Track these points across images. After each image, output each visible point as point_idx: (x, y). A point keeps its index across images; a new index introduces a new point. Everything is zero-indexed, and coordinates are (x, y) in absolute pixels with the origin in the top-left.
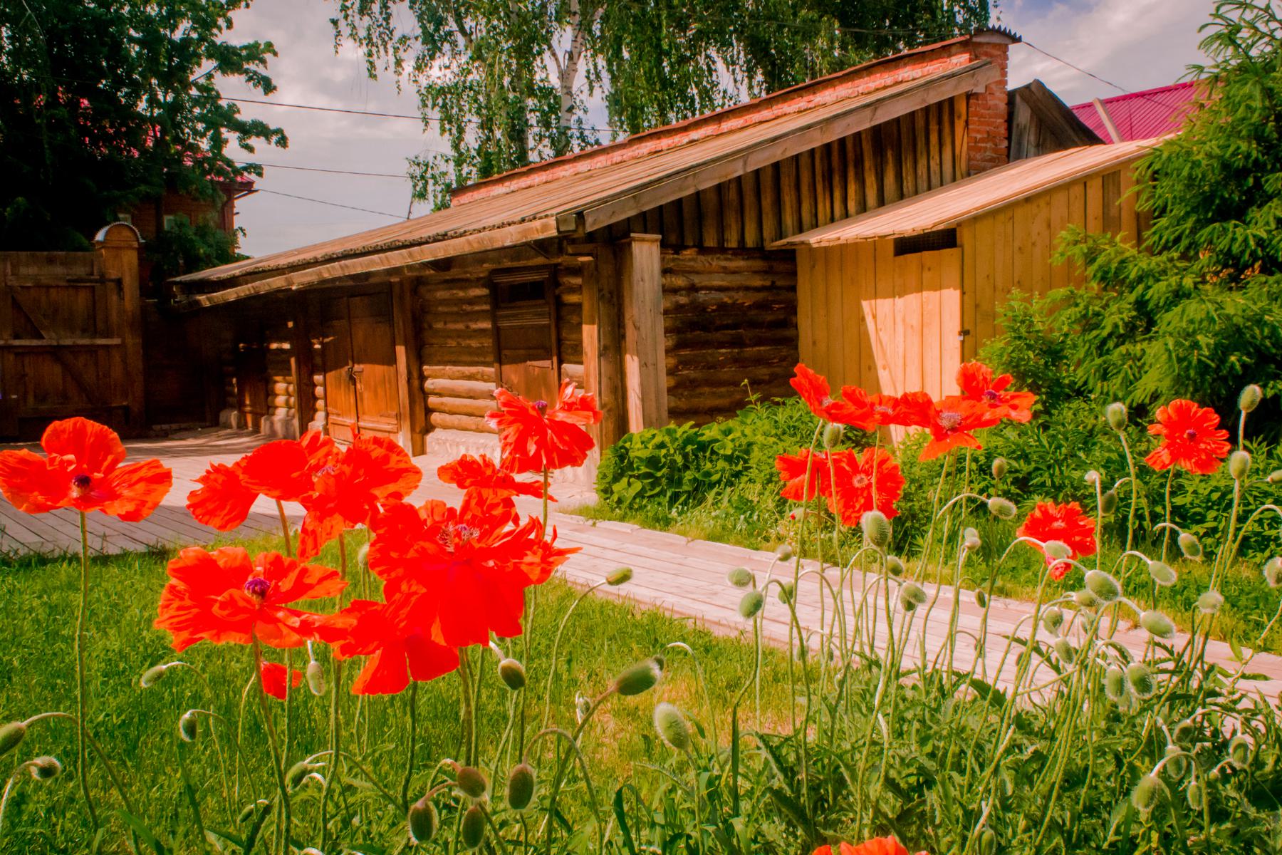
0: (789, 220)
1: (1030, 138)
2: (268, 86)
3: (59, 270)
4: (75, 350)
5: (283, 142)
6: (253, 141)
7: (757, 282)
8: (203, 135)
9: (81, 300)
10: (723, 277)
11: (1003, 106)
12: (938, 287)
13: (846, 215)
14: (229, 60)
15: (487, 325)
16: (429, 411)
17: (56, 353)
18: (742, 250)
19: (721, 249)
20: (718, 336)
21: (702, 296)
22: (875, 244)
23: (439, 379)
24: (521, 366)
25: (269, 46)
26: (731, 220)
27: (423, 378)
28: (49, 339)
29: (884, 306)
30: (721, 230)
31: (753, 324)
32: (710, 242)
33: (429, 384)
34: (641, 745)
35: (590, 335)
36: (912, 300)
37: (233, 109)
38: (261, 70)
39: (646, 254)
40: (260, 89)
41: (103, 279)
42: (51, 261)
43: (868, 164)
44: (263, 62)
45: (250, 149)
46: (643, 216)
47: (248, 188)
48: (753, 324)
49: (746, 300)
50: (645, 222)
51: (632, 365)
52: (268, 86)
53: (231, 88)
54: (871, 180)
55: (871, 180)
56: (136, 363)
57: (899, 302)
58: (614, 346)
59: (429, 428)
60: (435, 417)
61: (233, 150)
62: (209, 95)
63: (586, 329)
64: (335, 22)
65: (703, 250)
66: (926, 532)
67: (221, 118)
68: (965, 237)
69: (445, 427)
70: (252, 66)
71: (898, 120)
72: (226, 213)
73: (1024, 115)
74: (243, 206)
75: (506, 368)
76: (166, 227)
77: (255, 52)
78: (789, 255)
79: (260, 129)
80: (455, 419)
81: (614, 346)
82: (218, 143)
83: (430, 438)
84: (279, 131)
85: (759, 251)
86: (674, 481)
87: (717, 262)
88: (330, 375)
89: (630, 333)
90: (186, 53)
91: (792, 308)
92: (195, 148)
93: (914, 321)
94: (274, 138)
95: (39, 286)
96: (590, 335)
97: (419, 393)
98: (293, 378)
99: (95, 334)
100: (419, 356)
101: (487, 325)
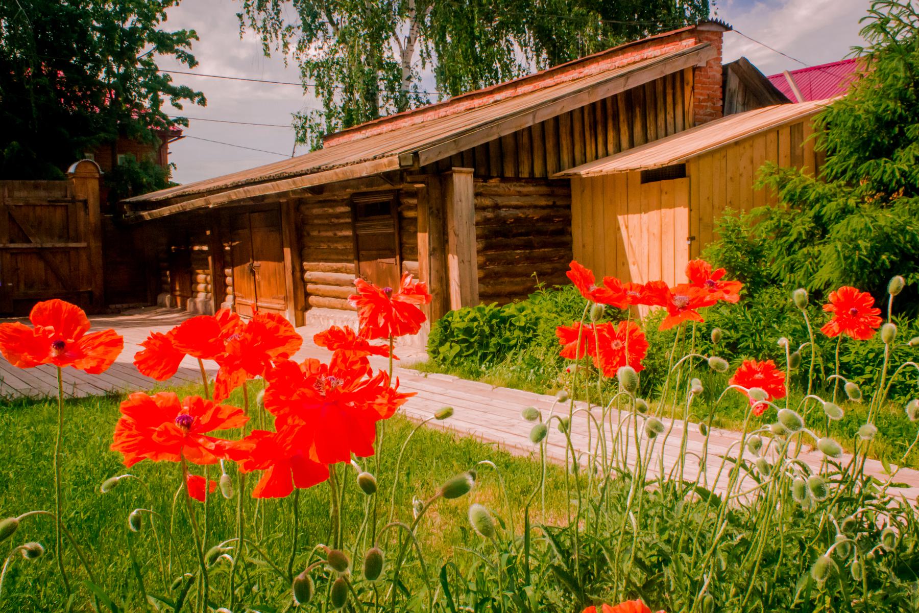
0: (565, 158)
1: (739, 99)
2: (192, 62)
3: (42, 194)
4: (54, 251)
5: (203, 102)
6: (181, 101)
7: (543, 202)
8: (145, 97)
9: (58, 215)
10: (518, 199)
11: (719, 76)
12: (672, 206)
13: (607, 154)
14: (164, 43)
15: (349, 233)
16: (307, 295)
17: (40, 253)
18: (532, 180)
19: (517, 179)
20: (515, 241)
21: (503, 212)
22: (627, 175)
23: (315, 272)
24: (374, 263)
25: (193, 33)
26: (524, 158)
27: (303, 271)
28: (35, 243)
29: (634, 219)
30: (517, 165)
31: (540, 233)
32: (509, 173)
33: (308, 275)
34: (460, 534)
35: (423, 240)
36: (654, 215)
37: (167, 78)
38: (187, 50)
39: (463, 182)
40: (187, 64)
41: (74, 200)
42: (36, 187)
43: (622, 117)
44: (189, 44)
45: (179, 107)
46: (461, 155)
47: (178, 135)
48: (540, 233)
49: (535, 215)
50: (463, 159)
51: (453, 262)
52: (192, 62)
53: (165, 63)
54: (624, 129)
55: (624, 129)
56: (98, 260)
57: (645, 216)
58: (440, 248)
59: (307, 307)
60: (312, 299)
61: (167, 107)
62: (150, 68)
63: (420, 236)
64: (240, 16)
65: (504, 179)
66: (664, 381)
67: (158, 84)
68: (692, 170)
69: (319, 306)
70: (180, 48)
71: (643, 86)
72: (162, 152)
73: (734, 83)
74: (174, 148)
75: (363, 264)
76: (119, 162)
77: (183, 37)
78: (566, 183)
79: (186, 93)
80: (326, 301)
81: (440, 248)
82: (156, 102)
83: (308, 314)
84: (200, 94)
85: (544, 180)
86: (483, 345)
87: (514, 188)
88: (237, 269)
89: (452, 239)
90: (133, 38)
91: (568, 221)
92: (139, 106)
93: (656, 230)
94: (197, 99)
95: (28, 205)
96: (423, 240)
97: (300, 282)
98: (210, 271)
99: (68, 239)
100: (301, 255)
101: (349, 233)
